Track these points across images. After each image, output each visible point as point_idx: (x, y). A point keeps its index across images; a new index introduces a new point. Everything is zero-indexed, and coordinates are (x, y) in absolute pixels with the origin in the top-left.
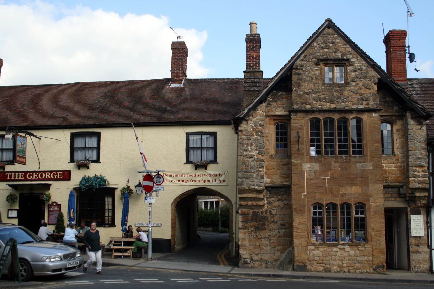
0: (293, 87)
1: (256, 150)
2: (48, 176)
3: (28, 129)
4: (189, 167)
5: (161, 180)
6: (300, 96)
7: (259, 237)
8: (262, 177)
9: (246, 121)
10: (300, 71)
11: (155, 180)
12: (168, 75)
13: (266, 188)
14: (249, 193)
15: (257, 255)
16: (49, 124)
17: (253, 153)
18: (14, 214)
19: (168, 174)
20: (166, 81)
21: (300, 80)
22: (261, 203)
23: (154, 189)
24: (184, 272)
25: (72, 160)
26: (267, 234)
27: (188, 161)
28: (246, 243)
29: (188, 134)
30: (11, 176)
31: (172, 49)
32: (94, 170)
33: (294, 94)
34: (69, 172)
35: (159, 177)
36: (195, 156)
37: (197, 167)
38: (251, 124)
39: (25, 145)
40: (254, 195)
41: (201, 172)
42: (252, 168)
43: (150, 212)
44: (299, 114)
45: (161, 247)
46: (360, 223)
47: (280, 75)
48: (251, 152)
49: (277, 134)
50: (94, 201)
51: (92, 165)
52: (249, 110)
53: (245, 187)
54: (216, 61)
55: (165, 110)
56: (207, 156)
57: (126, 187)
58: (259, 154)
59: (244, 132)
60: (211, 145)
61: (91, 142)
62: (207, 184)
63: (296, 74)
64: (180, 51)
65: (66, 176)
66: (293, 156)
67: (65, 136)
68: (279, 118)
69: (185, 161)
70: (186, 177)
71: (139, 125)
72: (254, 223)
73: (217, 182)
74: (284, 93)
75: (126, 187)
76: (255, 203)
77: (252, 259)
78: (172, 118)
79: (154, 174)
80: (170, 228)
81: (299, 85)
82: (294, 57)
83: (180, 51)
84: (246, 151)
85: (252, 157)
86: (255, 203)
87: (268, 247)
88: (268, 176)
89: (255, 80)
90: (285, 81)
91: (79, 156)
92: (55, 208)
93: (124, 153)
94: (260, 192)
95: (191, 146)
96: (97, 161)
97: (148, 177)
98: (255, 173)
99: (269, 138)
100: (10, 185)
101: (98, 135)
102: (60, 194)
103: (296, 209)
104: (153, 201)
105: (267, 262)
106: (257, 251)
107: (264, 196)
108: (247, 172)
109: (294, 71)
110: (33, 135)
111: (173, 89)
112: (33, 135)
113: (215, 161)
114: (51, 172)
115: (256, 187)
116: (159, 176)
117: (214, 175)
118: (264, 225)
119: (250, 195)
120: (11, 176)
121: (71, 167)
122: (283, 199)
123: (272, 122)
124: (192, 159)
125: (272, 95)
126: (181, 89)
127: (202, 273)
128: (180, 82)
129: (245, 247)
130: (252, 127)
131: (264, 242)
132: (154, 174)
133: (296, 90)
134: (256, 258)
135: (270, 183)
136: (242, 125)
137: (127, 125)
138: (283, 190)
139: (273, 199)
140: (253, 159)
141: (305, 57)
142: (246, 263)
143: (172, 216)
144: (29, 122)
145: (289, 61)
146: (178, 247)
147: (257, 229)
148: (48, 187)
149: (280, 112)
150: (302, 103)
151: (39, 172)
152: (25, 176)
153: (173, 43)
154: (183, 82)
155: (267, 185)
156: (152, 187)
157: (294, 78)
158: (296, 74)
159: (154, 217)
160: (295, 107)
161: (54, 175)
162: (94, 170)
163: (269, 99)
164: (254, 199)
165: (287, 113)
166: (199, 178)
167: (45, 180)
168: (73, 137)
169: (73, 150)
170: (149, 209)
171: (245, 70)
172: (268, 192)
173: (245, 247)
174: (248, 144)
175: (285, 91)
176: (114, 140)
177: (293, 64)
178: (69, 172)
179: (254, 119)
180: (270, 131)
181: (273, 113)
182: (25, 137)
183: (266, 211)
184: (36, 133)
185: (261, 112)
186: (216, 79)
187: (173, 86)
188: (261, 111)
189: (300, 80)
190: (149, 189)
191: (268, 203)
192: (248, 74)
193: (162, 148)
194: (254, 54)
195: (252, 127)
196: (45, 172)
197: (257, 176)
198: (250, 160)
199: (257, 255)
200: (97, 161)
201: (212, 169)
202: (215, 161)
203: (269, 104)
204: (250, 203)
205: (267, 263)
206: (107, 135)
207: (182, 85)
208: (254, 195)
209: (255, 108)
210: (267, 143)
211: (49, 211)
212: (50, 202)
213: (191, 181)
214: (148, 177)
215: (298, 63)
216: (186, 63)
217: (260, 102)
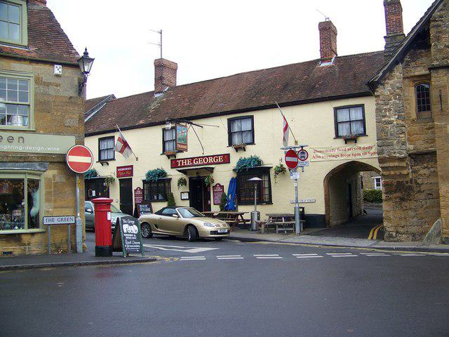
0: (431, 42)
1: (395, 115)
2: (211, 160)
3: (189, 120)
4: (340, 142)
5: (306, 155)
6: (440, 51)
7: (404, 208)
8: (404, 143)
9: (383, 85)
10: (440, 23)
11: (299, 155)
12: (318, 56)
13: (410, 155)
14: (391, 161)
15: (403, 227)
16: (208, 112)
17: (392, 119)
18: (186, 196)
19: (319, 150)
20: (315, 62)
21: (440, 32)
22: (405, 172)
23: (299, 165)
24: (322, 247)
25: (230, 144)
26: (413, 204)
27: (337, 136)
28: (391, 215)
29: (336, 109)
30: (181, 163)
31: (320, 30)
32: (251, 152)
33: (433, 50)
34: (229, 155)
35: (303, 153)
36: (344, 131)
37: (347, 140)
38: (388, 87)
39: (186, 134)
40: (396, 164)
41: (349, 146)
42: (391, 135)
43: (296, 187)
44: (440, 71)
45: (310, 223)
46: (18, 84)
47: (415, 30)
48: (389, 117)
49: (418, 96)
50: (253, 181)
51: (248, 147)
52: (384, 73)
53: (386, 155)
54: (364, 35)
55: (313, 87)
56: (356, 128)
57: (279, 166)
58: (398, 118)
59: (381, 97)
60: (360, 117)
61: (246, 125)
62: (358, 157)
63: (434, 26)
64: (327, 31)
65: (226, 159)
66: (436, 118)
67: (222, 122)
68: (419, 79)
69: (334, 136)
70: (336, 152)
71: (283, 105)
72: (398, 194)
73: (368, 156)
74: (423, 51)
75: (279, 166)
76: (397, 172)
77: (397, 232)
78: (319, 95)
79: (297, 150)
80: (324, 201)
81: (438, 39)
82: (430, 8)
83: (327, 31)
84: (384, 116)
85: (391, 122)
86: (397, 172)
87: (415, 219)
88: (411, 142)
89: (396, 44)
90: (422, 36)
91: (237, 140)
92: (219, 189)
93: (270, 135)
94: (401, 159)
95: (339, 120)
96: (253, 143)
97: (291, 153)
98: (395, 140)
99: (409, 102)
100: (179, 171)
101: (252, 118)
102: (223, 176)
103: (442, 177)
104: (298, 177)
105: (414, 235)
106: (403, 223)
107: (407, 164)
108: (387, 139)
109: (432, 23)
110: (192, 123)
111: (323, 67)
112: (192, 123)
113: (364, 134)
114: (213, 156)
115: (398, 155)
116: (303, 152)
117: (364, 148)
118: (409, 195)
119: (391, 164)
120: (181, 163)
121: (231, 150)
122: (430, 166)
123: (412, 84)
124: (340, 134)
125: (411, 54)
126: (330, 67)
127: (312, 246)
128: (329, 60)
129: (389, 219)
130: (389, 91)
131: (412, 213)
132: (297, 150)
133: (435, 45)
134: (402, 230)
135: (414, 149)
136: (377, 89)
137: (273, 107)
138: (429, 156)
139: (418, 167)
140: (392, 125)
141: (445, 5)
142: (391, 236)
143: (325, 192)
144: (193, 113)
145: (426, 14)
146: (333, 222)
147: (402, 199)
148: (212, 170)
149: (422, 71)
150: (444, 58)
151: (203, 157)
152: (192, 162)
153: (320, 23)
154: (332, 60)
155: (410, 152)
156: (296, 163)
157: (433, 32)
158: (434, 26)
159: (305, 192)
160: (435, 63)
161: (206, 160)
162: (251, 152)
163: (407, 59)
164: (397, 168)
165: (428, 72)
166: (350, 152)
167: (208, 164)
168: (230, 122)
169: (231, 134)
170: (295, 185)
171: (386, 35)
172: (412, 160)
173: (389, 219)
174: (385, 109)
175: (424, 49)
176: (267, 124)
177: (431, 16)
178: (229, 155)
179: (391, 82)
180: (411, 93)
181: (412, 74)
182: (186, 126)
183: (411, 180)
184: (194, 122)
185: (398, 74)
186: (365, 54)
187: (323, 65)
188: (398, 73)
189: (440, 32)
190: (292, 165)
191: (412, 172)
192: (389, 39)
193: (313, 125)
194: (394, 18)
195: (389, 91)
196: (208, 157)
197: (398, 142)
198: (389, 126)
199: (403, 227)
200: (253, 143)
201: (363, 142)
202: (364, 134)
203: (408, 65)
204: (392, 173)
205: (414, 236)
206: (259, 117)
207: (330, 64)
208: (396, 164)
209: (390, 70)
210: (408, 107)
211: (214, 192)
212: (214, 184)
213: (342, 155)
214: (291, 153)
215: (437, 13)
216: (336, 42)
217: (396, 63)
